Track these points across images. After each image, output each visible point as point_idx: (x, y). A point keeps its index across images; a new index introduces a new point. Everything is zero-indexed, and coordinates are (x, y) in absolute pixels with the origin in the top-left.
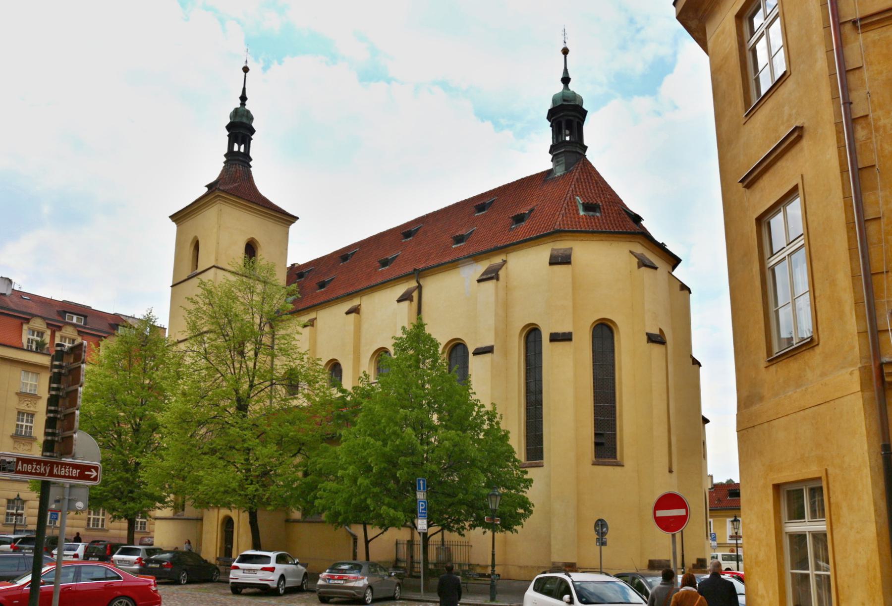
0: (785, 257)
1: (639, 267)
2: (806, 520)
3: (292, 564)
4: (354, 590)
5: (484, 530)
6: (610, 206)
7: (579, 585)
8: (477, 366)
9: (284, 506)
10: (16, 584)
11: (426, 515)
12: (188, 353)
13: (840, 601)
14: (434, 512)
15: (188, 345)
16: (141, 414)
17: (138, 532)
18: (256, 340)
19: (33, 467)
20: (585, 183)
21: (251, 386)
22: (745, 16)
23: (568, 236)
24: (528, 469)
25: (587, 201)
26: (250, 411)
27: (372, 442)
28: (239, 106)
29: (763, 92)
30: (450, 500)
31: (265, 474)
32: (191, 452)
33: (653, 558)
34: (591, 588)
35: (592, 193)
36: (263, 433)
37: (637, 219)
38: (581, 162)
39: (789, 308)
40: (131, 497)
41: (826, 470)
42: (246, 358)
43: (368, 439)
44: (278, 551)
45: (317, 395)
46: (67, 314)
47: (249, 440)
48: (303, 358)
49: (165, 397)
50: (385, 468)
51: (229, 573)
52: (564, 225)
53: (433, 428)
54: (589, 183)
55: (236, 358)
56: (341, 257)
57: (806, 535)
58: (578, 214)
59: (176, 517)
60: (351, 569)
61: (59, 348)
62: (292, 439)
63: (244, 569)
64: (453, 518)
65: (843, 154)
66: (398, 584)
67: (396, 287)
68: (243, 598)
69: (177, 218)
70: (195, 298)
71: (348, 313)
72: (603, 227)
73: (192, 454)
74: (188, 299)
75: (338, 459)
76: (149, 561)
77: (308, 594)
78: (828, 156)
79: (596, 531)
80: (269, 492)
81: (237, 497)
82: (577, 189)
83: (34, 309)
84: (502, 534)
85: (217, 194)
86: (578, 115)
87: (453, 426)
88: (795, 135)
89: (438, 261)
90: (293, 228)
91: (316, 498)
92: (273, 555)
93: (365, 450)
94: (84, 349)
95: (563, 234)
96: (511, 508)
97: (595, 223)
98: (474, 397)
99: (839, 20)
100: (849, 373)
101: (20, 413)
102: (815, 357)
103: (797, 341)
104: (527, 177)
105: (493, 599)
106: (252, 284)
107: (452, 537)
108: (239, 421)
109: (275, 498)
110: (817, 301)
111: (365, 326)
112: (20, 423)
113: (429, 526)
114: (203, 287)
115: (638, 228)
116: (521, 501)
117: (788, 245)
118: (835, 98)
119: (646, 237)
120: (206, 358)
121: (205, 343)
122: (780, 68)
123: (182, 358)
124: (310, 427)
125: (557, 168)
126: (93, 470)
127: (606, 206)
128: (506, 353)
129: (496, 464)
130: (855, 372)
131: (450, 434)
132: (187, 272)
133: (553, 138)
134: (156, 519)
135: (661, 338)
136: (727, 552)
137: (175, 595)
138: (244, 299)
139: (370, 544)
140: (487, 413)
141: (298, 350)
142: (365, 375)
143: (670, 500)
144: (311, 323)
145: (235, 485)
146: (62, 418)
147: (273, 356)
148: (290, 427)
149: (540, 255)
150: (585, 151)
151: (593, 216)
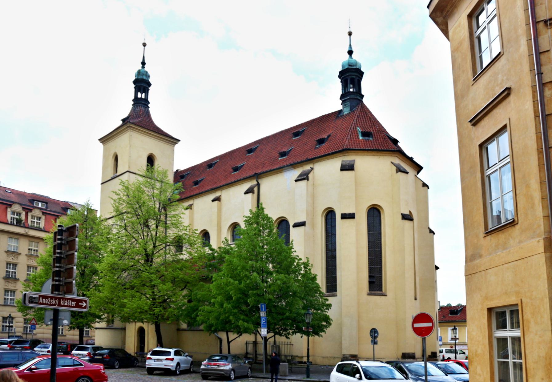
0: (497, 169)
1: (397, 172)
2: (508, 329)
3: (183, 356)
4: (223, 372)
5: (301, 335)
6: (379, 133)
7: (364, 369)
8: (295, 234)
9: (177, 321)
10: (19, 369)
11: (266, 326)
12: (114, 226)
13: (528, 377)
14: (271, 324)
15: (114, 221)
16: (85, 264)
17: (85, 337)
18: (157, 218)
19: (48, 301)
20: (363, 118)
21: (155, 247)
22: (474, 15)
23: (352, 152)
24: (328, 298)
25: (364, 130)
26: (154, 262)
27: (232, 282)
28: (140, 68)
29: (484, 66)
30: (281, 317)
31: (165, 301)
32: (118, 288)
33: (404, 352)
34: (371, 370)
35: (367, 125)
36: (163, 276)
37: (395, 142)
38: (360, 105)
39: (500, 200)
40: (81, 315)
41: (521, 300)
42: (151, 229)
43: (230, 280)
44: (175, 348)
45: (196, 252)
46: (35, 202)
47: (155, 280)
48: (187, 229)
49: (100, 254)
50: (240, 298)
51: (145, 362)
52: (349, 145)
53: (270, 273)
54: (365, 119)
55: (144, 230)
56: (208, 165)
57: (507, 339)
58: (359, 138)
59: (108, 328)
60: (221, 359)
61: (60, 228)
62: (181, 279)
63: (155, 360)
64: (282, 328)
65: (536, 106)
66: (250, 368)
67: (243, 184)
68: (155, 377)
69: (104, 140)
70: (118, 192)
71: (213, 201)
72: (374, 147)
73: (119, 289)
74: (114, 192)
75: (211, 292)
76: (95, 355)
77: (194, 374)
78: (527, 107)
79: (371, 335)
80: (168, 312)
81: (148, 316)
82: (358, 123)
83: (14, 198)
84: (313, 337)
85: (128, 125)
86: (358, 75)
87: (282, 271)
88: (506, 93)
89: (269, 168)
90: (177, 146)
91: (197, 316)
92: (172, 351)
93: (228, 286)
94: (77, 229)
95: (349, 151)
96: (318, 322)
97: (369, 144)
98: (295, 254)
99: (535, 20)
100: (537, 241)
101: (8, 264)
102: (515, 231)
103: (504, 221)
104: (326, 115)
105: (308, 377)
106: (153, 183)
107: (280, 339)
108: (148, 269)
109: (171, 316)
110: (517, 197)
111: (224, 209)
112: (8, 270)
113: (268, 333)
114: (123, 184)
115: (396, 147)
116: (325, 318)
117: (499, 162)
118: (532, 70)
119: (401, 153)
120: (126, 229)
121: (124, 220)
122: (496, 50)
123: (111, 229)
124: (192, 272)
125: (345, 109)
126: (84, 302)
127: (376, 133)
128: (313, 226)
129: (309, 295)
130: (541, 241)
131: (281, 276)
132: (110, 175)
133: (342, 90)
134: (96, 329)
135: (411, 217)
136: (448, 348)
137: (113, 375)
138: (149, 192)
139: (231, 344)
140: (304, 263)
141: (183, 224)
142: (226, 240)
143: (422, 317)
144: (190, 207)
145: (146, 308)
146: (64, 271)
147: (166, 228)
148: (180, 272)
149: (336, 163)
150: (362, 98)
151: (368, 140)
